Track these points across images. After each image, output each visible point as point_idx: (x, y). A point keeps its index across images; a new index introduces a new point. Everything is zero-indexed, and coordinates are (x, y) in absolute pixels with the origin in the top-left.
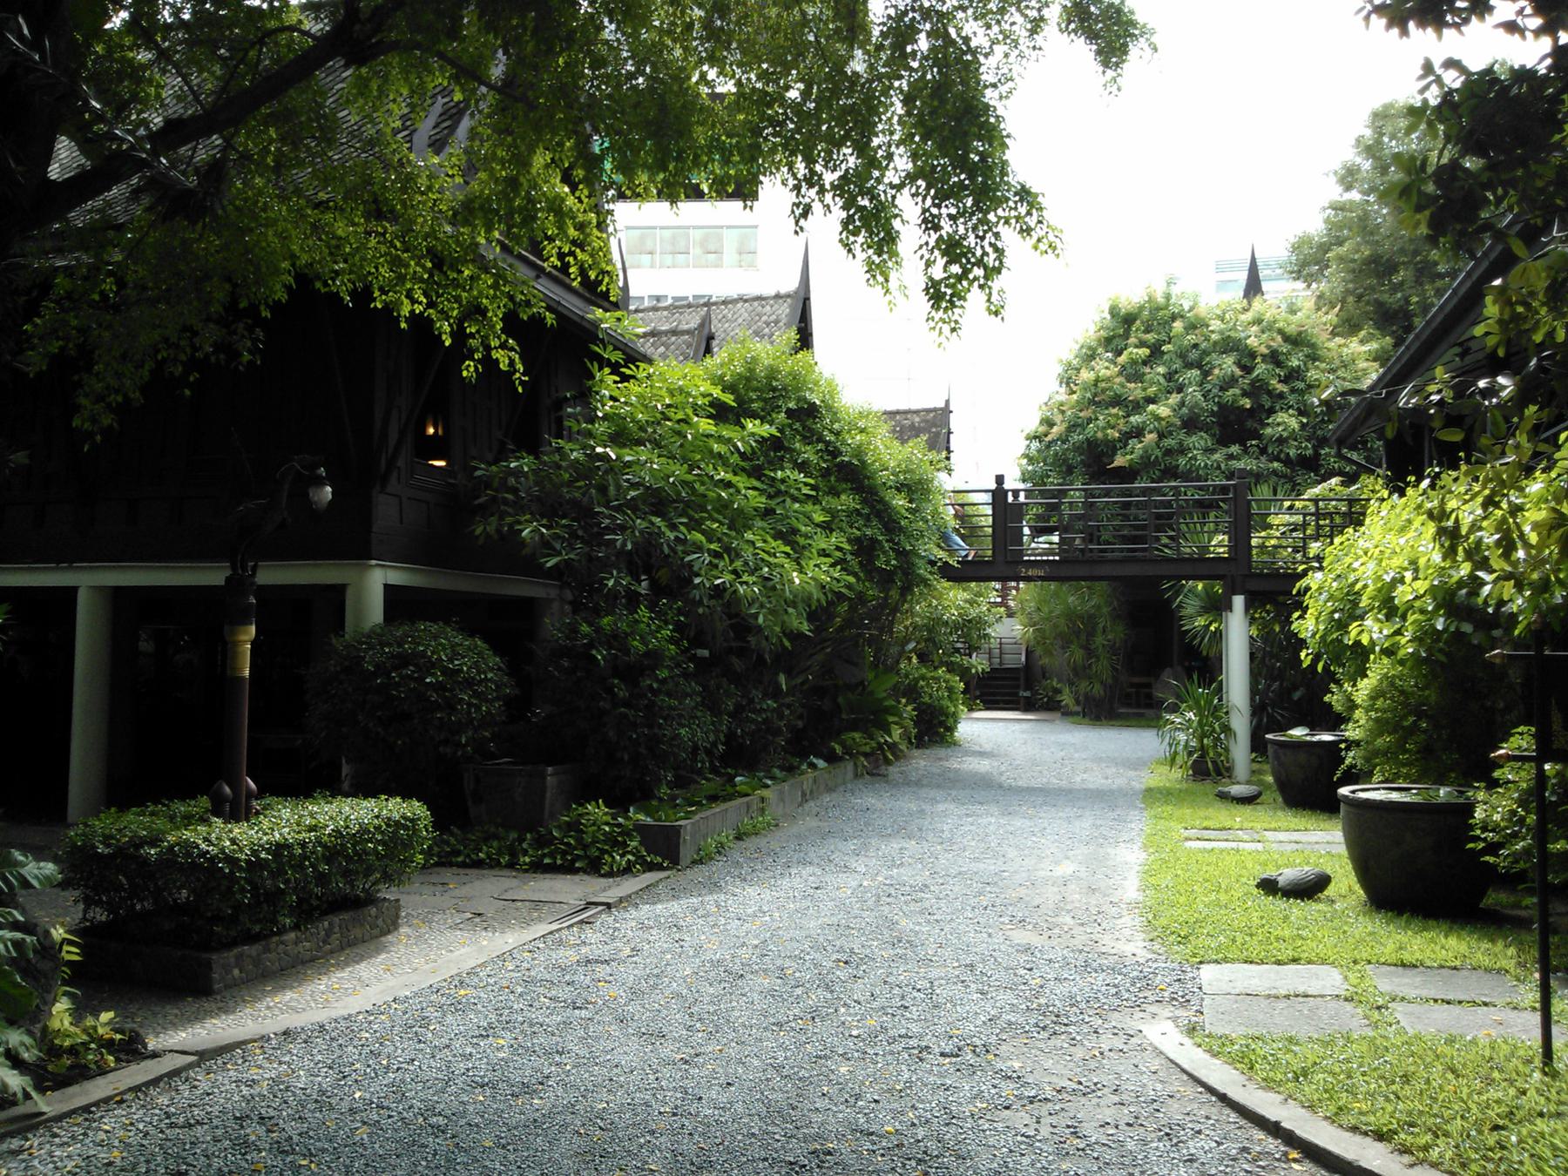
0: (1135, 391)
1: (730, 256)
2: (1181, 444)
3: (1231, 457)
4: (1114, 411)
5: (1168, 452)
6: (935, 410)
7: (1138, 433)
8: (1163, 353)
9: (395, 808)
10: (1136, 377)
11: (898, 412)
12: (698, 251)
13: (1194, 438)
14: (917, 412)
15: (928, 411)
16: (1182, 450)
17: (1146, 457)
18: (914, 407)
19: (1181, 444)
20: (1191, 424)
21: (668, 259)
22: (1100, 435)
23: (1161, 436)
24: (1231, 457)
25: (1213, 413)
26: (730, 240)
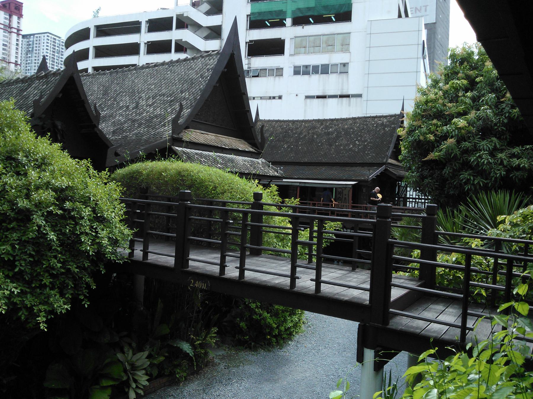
0: (451, 107)
1: (338, 46)
2: (475, 146)
3: (513, 156)
4: (435, 121)
5: (466, 151)
6: (395, 115)
7: (445, 137)
8: (477, 83)
9: (436, 205)
10: (454, 99)
11: (376, 117)
12: (324, 45)
13: (484, 143)
14: (385, 117)
15: (391, 116)
16: (476, 149)
17: (448, 152)
18: (281, 119)
19: (475, 146)
20: (486, 130)
21: (312, 49)
22: (421, 138)
23: (458, 142)
24: (513, 156)
25: (504, 124)
26: (338, 41)
